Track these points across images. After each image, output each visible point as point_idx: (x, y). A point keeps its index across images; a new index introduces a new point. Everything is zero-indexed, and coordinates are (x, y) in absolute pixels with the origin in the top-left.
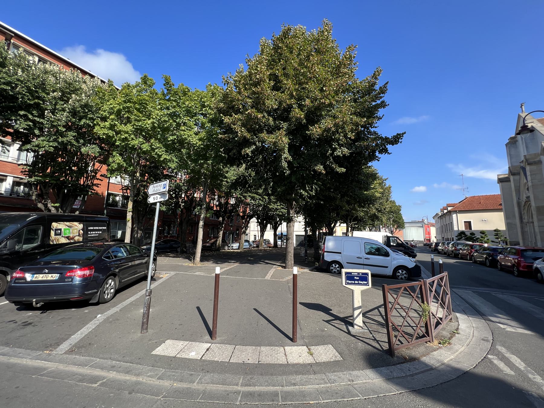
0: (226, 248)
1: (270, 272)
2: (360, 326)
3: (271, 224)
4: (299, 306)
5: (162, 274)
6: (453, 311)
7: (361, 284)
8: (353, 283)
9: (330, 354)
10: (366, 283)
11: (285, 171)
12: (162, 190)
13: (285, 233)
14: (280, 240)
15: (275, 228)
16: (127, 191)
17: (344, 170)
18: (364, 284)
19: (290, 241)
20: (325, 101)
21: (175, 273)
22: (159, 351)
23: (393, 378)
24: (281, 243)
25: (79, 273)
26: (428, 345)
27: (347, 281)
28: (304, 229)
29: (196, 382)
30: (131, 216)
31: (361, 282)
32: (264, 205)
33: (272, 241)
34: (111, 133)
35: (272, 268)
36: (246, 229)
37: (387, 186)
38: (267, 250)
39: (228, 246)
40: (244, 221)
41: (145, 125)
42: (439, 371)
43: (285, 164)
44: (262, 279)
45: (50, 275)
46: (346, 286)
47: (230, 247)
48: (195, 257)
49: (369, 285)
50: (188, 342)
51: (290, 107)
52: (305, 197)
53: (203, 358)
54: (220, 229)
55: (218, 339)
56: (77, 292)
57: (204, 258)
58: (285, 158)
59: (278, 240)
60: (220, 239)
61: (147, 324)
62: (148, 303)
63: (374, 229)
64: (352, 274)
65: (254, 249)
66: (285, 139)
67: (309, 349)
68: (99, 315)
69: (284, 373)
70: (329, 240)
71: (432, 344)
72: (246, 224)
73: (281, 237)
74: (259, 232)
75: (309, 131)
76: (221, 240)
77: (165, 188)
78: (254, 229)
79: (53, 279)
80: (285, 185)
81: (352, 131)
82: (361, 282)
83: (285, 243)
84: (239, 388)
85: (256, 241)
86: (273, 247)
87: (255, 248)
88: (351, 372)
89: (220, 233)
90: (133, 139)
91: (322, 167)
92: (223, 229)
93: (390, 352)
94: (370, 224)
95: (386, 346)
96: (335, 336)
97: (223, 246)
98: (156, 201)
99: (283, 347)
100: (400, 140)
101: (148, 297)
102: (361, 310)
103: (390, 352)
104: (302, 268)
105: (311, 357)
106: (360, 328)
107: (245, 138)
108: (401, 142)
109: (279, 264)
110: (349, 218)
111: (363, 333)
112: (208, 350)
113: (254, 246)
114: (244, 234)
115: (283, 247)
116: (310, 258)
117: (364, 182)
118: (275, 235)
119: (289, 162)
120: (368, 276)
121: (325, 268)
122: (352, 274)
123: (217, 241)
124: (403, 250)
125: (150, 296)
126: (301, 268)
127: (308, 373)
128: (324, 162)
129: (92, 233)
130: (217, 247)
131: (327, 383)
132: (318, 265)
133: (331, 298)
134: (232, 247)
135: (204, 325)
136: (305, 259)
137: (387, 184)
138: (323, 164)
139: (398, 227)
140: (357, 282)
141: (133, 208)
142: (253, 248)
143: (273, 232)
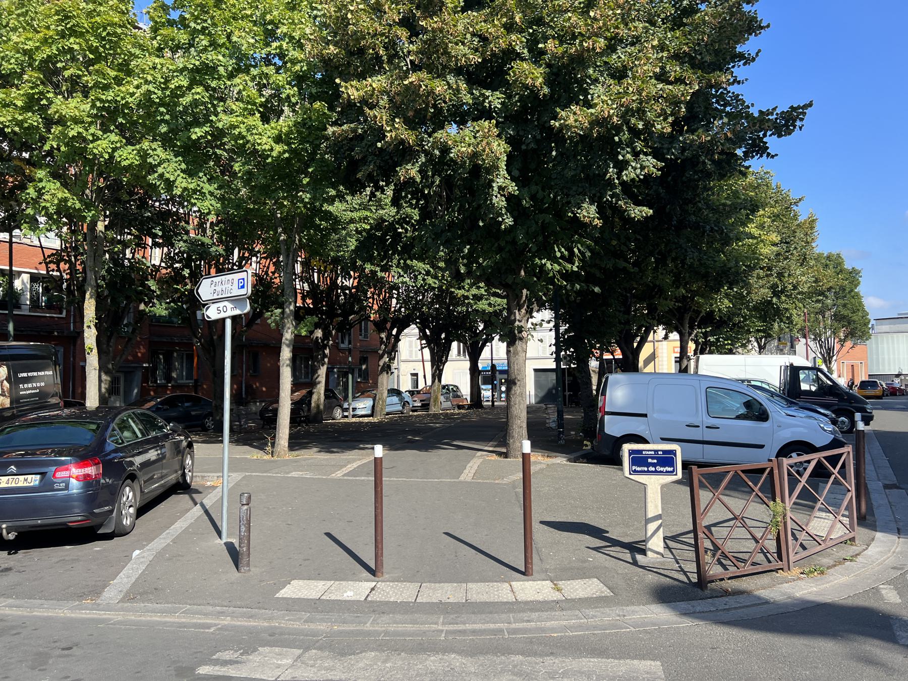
0: (338, 413)
1: (469, 465)
2: (658, 553)
3: (459, 341)
4: (536, 527)
5: (210, 479)
6: (859, 524)
7: (661, 472)
8: (644, 471)
9: (592, 590)
10: (671, 469)
11: (500, 219)
12: (236, 292)
13: (502, 364)
14: (490, 387)
15: (474, 354)
16: (58, 266)
17: (647, 211)
18: (667, 472)
19: (516, 389)
20: (593, 44)
21: (243, 474)
22: (287, 592)
23: (694, 613)
24: (493, 395)
25: (75, 471)
26: (778, 575)
27: (634, 468)
28: (554, 355)
29: (370, 622)
30: (94, 339)
31: (662, 469)
32: (440, 288)
33: (465, 390)
34: (33, 119)
35: (474, 456)
36: (392, 359)
37: (801, 219)
38: (453, 414)
39: (341, 406)
40: (383, 335)
41: (123, 98)
42: (778, 605)
43: (499, 201)
44: (452, 480)
45: (22, 478)
46: (631, 477)
47: (346, 410)
48: (275, 437)
49: (676, 475)
50: (332, 582)
51: (510, 54)
52: (554, 276)
53: (369, 599)
54: (318, 362)
55: (386, 576)
56: (77, 511)
57: (296, 443)
58: (500, 188)
59: (483, 387)
60: (321, 388)
61: (249, 554)
62: (247, 519)
63: (776, 342)
64: (644, 453)
65: (416, 413)
66: (499, 145)
67: (555, 585)
68: (137, 552)
69: (510, 611)
70: (617, 383)
71: (786, 574)
72: (390, 345)
73: (492, 376)
74: (428, 365)
75: (555, 118)
76: (322, 392)
77: (243, 287)
78: (411, 356)
79: (28, 485)
80: (500, 250)
81: (664, 114)
82: (662, 469)
83: (503, 395)
84: (440, 628)
85: (418, 392)
86: (470, 407)
87: (416, 411)
88: (624, 608)
89: (320, 372)
90: (96, 139)
91: (593, 208)
92: (326, 360)
93: (703, 582)
94: (758, 331)
95: (694, 578)
96: (605, 567)
97: (330, 408)
98: (222, 315)
99: (509, 582)
100: (798, 123)
101: (245, 507)
102: (660, 521)
103: (703, 582)
104: (550, 455)
105: (557, 593)
106: (659, 556)
107: (402, 142)
108: (801, 128)
109: (491, 449)
110: (687, 318)
111: (662, 563)
112: (373, 589)
113: (416, 405)
114: (385, 373)
115: (499, 407)
116: (573, 433)
117: (712, 230)
118: (474, 371)
119: (510, 198)
120: (675, 456)
121: (607, 452)
122: (644, 453)
123: (310, 394)
124: (833, 405)
125: (248, 504)
126: (548, 456)
127: (552, 609)
128: (598, 194)
129: (26, 386)
130: (314, 410)
131: (581, 619)
132: (589, 447)
133: (611, 513)
134: (354, 409)
135: (351, 558)
136: (559, 434)
137: (803, 213)
138: (596, 199)
139: (851, 334)
140: (653, 469)
141: (98, 317)
142: (413, 411)
143: (467, 364)
